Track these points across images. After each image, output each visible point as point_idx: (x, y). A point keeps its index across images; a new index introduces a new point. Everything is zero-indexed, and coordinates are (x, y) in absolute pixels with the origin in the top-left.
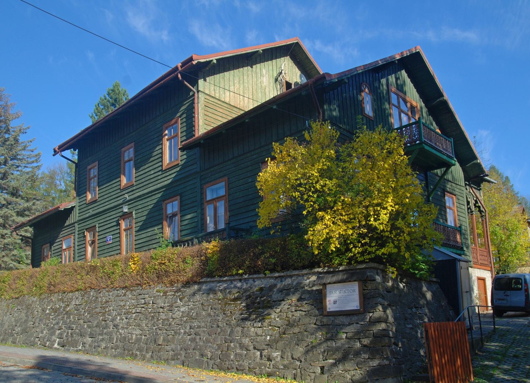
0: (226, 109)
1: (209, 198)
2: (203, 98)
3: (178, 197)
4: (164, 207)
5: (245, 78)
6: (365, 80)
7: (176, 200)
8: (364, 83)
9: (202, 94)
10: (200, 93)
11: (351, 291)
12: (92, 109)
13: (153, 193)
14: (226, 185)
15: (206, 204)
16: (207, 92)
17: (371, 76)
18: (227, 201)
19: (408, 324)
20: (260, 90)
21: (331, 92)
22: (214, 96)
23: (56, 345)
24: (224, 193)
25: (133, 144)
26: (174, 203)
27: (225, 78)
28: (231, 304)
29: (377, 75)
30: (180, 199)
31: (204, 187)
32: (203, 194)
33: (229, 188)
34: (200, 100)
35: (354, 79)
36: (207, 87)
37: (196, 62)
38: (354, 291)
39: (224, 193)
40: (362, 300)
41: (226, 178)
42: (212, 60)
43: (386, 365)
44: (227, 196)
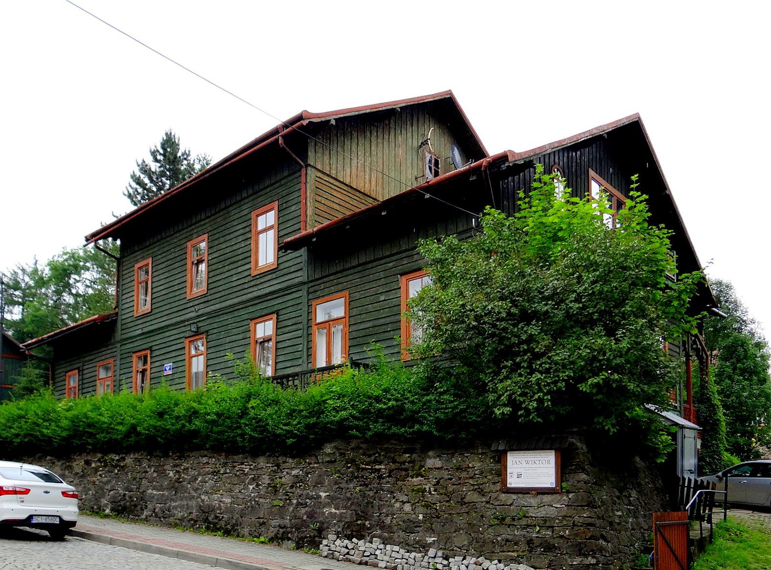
0: (345, 193)
1: (320, 318)
2: (313, 176)
3: (275, 316)
4: (252, 328)
5: (373, 148)
6: (557, 160)
7: (271, 319)
8: (556, 166)
9: (313, 169)
10: (309, 168)
11: (544, 462)
12: (125, 183)
13: (236, 308)
14: (345, 303)
15: (315, 328)
16: (319, 167)
17: (566, 155)
18: (347, 325)
19: (618, 511)
20: (393, 168)
21: (510, 178)
22: (328, 173)
23: (107, 511)
24: (342, 314)
25: (206, 236)
26: (266, 323)
27: (345, 147)
28: (367, 469)
29: (574, 154)
30: (277, 318)
31: (314, 303)
32: (310, 313)
33: (350, 305)
34: (308, 178)
35: (552, 156)
36: (321, 160)
37: (307, 121)
38: (549, 462)
39: (342, 314)
40: (559, 476)
41: (346, 293)
42: (330, 121)
43: (591, 564)
44: (347, 318)
